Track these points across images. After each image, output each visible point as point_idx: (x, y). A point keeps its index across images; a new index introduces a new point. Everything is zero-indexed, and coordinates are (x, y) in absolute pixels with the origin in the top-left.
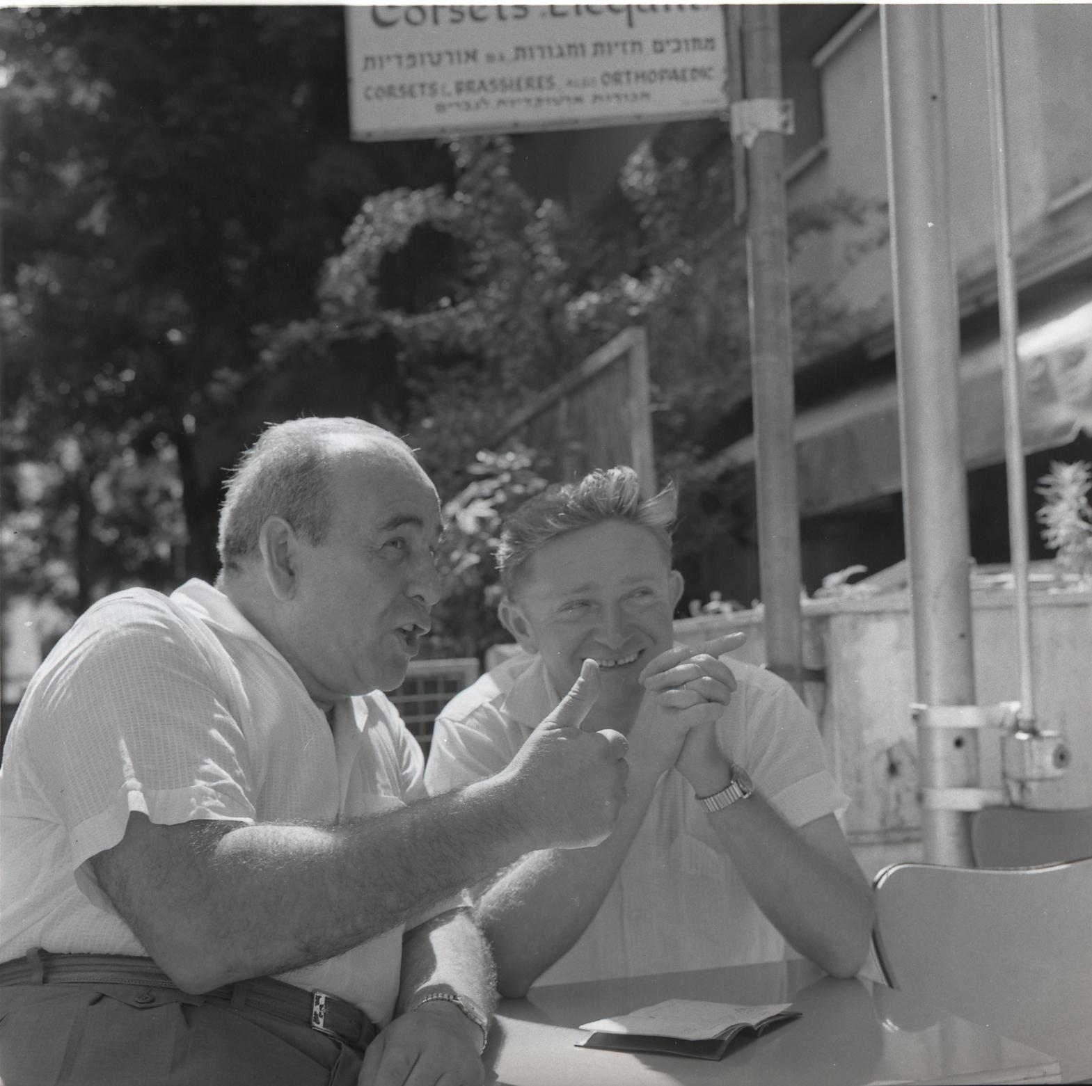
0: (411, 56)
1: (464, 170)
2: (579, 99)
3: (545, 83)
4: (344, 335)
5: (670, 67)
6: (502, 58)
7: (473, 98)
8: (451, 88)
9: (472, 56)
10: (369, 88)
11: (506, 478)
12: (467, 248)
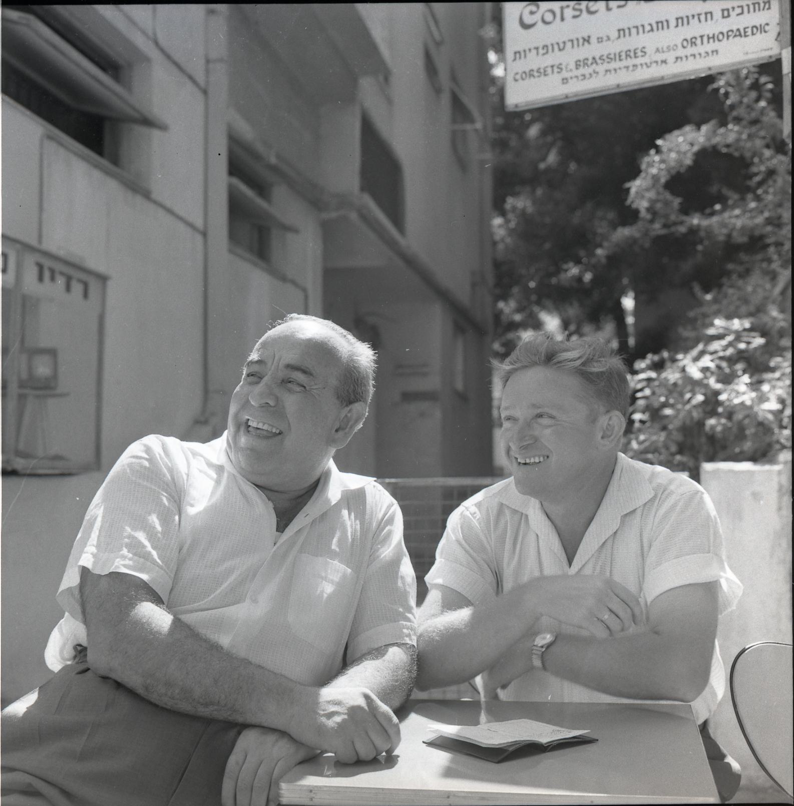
0: (545, 47)
1: (732, 107)
2: (664, 62)
3: (640, 54)
4: (664, 232)
5: (535, 67)
6: (608, 39)
7: (586, 71)
8: (572, 66)
9: (587, 40)
10: (517, 74)
11: (730, 338)
12: (747, 164)
